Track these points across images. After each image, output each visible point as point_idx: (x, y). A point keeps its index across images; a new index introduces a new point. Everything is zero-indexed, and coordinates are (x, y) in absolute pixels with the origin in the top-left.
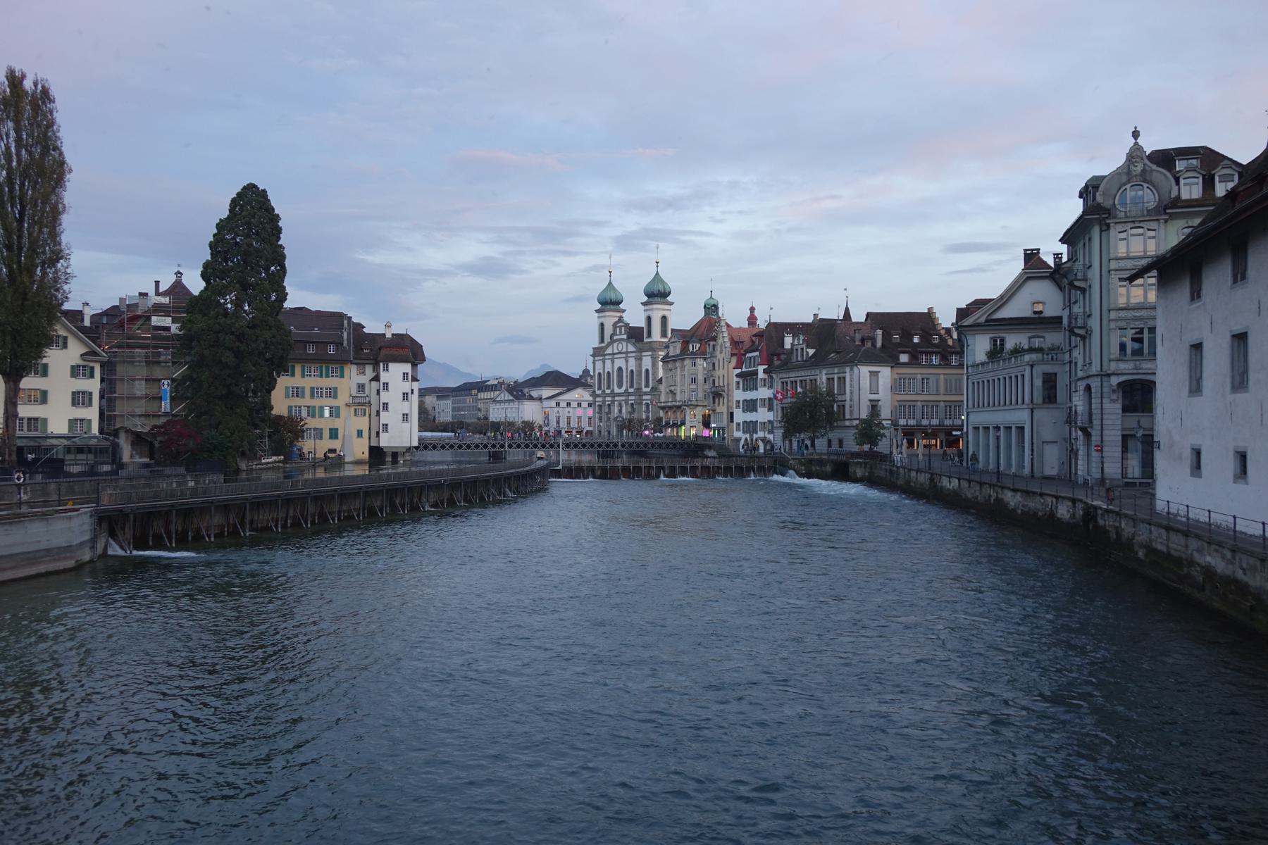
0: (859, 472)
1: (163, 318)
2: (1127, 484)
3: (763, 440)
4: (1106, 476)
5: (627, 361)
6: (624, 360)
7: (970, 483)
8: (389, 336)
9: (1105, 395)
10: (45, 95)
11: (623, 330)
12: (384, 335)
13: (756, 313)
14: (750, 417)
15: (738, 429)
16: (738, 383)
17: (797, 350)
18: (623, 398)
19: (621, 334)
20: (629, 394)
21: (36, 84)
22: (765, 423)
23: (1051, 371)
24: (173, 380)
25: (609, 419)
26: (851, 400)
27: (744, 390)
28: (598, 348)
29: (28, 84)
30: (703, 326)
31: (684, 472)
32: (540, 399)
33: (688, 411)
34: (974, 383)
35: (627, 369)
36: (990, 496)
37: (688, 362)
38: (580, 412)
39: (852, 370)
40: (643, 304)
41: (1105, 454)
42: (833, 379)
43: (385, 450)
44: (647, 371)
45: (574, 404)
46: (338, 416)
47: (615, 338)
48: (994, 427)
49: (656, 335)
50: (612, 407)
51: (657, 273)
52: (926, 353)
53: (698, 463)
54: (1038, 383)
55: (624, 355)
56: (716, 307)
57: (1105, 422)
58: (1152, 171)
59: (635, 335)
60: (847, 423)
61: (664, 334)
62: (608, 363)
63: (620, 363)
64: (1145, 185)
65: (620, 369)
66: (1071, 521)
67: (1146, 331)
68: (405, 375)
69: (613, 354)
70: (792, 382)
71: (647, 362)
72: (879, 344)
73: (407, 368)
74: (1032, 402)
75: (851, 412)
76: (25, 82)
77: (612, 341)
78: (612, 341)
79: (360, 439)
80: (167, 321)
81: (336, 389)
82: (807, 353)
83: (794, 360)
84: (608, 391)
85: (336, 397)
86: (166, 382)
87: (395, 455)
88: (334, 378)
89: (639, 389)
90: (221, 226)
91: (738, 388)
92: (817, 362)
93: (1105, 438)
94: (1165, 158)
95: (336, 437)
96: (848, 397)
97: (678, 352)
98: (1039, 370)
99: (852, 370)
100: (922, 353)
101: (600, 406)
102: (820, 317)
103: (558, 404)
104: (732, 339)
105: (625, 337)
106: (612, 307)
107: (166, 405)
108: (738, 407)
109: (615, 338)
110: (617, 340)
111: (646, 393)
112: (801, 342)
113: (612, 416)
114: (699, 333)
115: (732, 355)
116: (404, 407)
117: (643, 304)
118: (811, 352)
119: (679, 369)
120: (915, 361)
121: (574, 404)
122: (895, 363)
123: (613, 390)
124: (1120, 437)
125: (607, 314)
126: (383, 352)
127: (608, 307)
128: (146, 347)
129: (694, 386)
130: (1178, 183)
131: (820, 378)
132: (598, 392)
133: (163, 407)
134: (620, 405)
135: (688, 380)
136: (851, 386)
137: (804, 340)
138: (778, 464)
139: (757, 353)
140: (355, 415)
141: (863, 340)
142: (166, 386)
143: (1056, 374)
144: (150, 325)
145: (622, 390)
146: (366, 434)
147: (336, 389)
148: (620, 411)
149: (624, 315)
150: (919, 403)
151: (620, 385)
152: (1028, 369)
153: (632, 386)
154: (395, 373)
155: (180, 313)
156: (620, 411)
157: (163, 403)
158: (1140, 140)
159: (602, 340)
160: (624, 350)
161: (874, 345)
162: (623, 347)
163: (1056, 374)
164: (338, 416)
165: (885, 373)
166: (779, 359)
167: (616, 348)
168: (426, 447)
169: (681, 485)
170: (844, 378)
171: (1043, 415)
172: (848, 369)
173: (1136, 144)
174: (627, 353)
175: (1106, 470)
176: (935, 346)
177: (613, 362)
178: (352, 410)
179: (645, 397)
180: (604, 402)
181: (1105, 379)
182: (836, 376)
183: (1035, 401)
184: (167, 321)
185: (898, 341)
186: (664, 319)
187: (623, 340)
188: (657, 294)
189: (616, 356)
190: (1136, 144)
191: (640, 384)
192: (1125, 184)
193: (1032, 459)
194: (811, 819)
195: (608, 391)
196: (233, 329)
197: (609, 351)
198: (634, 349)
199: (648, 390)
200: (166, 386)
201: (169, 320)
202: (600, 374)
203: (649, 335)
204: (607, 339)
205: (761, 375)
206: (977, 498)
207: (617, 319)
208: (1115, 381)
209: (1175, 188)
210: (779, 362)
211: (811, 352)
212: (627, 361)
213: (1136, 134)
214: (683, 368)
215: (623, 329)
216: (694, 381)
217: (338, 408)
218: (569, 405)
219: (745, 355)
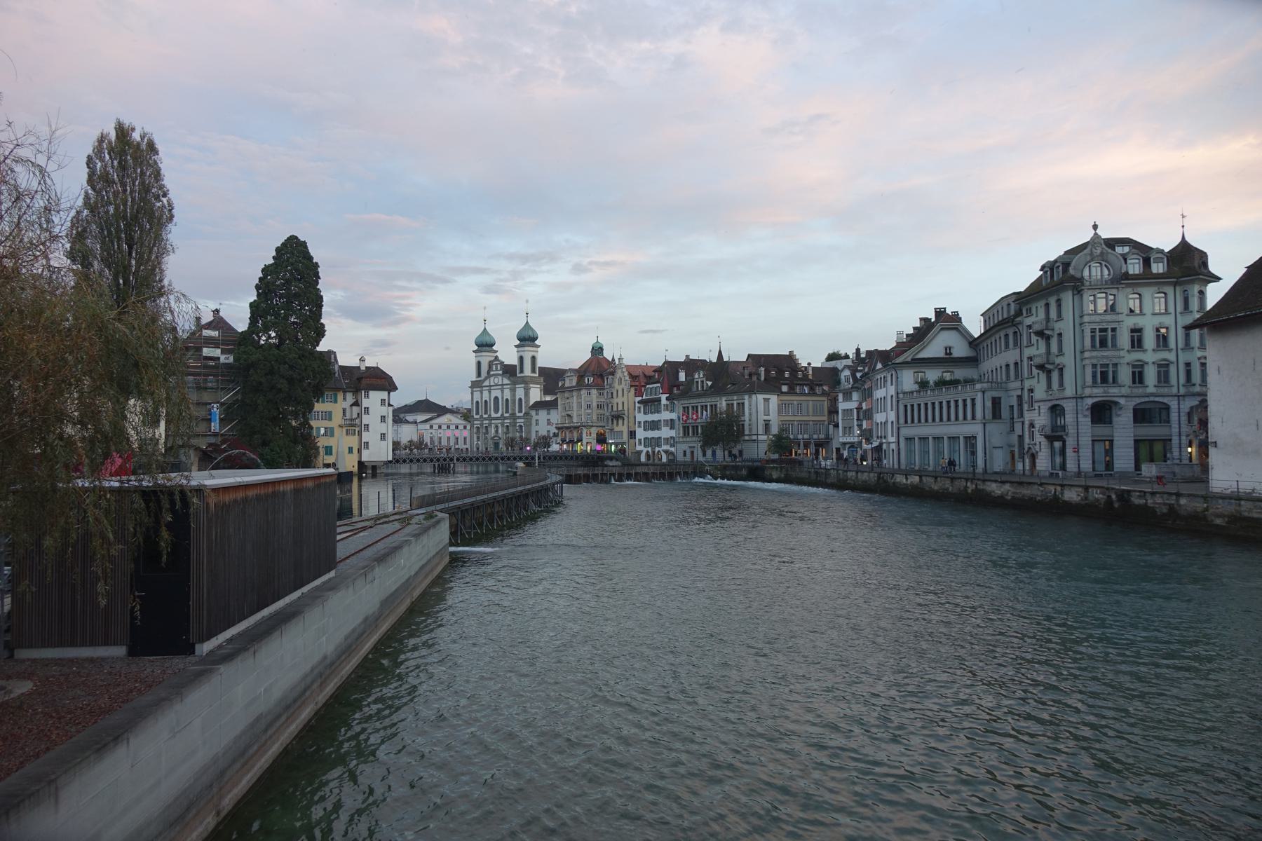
0: (775, 475)
1: (213, 349)
2: (1096, 476)
3: (666, 452)
4: (1082, 470)
5: (503, 392)
6: (500, 390)
7: (936, 478)
8: (363, 368)
9: (1079, 412)
10: (152, 147)
11: (499, 368)
12: (359, 367)
15: (640, 444)
16: (639, 408)
17: (697, 382)
19: (497, 370)
20: (506, 418)
21: (142, 138)
22: (667, 439)
23: (997, 396)
24: (222, 404)
25: (486, 438)
26: (750, 420)
27: (645, 413)
28: (476, 381)
29: (136, 136)
30: (593, 363)
31: (629, 477)
32: (415, 423)
33: (585, 431)
34: (906, 406)
35: (503, 398)
36: (966, 487)
37: (584, 392)
38: (457, 433)
39: (750, 397)
40: (516, 346)
41: (1080, 454)
42: (733, 404)
43: (366, 464)
44: (520, 400)
45: (444, 427)
46: (332, 435)
47: (492, 373)
48: (934, 438)
49: (527, 371)
51: (527, 322)
52: (800, 385)
53: (599, 471)
54: (989, 404)
56: (601, 349)
57: (1080, 431)
58: (1108, 253)
59: (509, 371)
60: (747, 438)
61: (533, 371)
62: (486, 394)
63: (496, 393)
64: (1104, 263)
65: (496, 398)
66: (1083, 503)
67: (1111, 366)
68: (383, 401)
69: (490, 386)
70: (693, 407)
71: (520, 393)
72: (763, 378)
73: (384, 395)
74: (984, 418)
75: (750, 430)
76: (134, 134)
77: (489, 376)
78: (489, 376)
79: (351, 455)
80: (217, 352)
81: (330, 413)
82: (707, 384)
83: (694, 389)
84: (485, 416)
85: (330, 419)
86: (215, 406)
87: (374, 468)
88: (329, 403)
89: (514, 414)
90: (266, 270)
91: (639, 412)
92: (717, 390)
93: (1080, 442)
94: (1112, 243)
95: (331, 454)
96: (747, 417)
97: (574, 383)
98: (989, 395)
99: (750, 397)
100: (797, 384)
101: (478, 428)
102: (691, 357)
103: (431, 427)
104: (630, 374)
105: (501, 372)
106: (487, 348)
107: (215, 426)
108: (640, 426)
109: (492, 373)
110: (493, 375)
111: (519, 418)
112: (701, 376)
113: (489, 436)
114: (591, 369)
115: (631, 386)
116: (382, 428)
117: (516, 346)
118: (710, 383)
119: (575, 398)
120: (792, 391)
121: (444, 427)
122: (776, 390)
123: (490, 415)
124: (1133, 442)
125: (484, 354)
126: (364, 382)
127: (484, 348)
128: (198, 374)
129: (589, 411)
130: (1126, 263)
131: (721, 404)
133: (213, 428)
134: (497, 427)
135: (584, 406)
136: (750, 409)
137: (704, 375)
138: (699, 471)
139: (659, 385)
140: (347, 434)
141: (750, 375)
142: (215, 409)
143: (1000, 398)
144: (201, 355)
145: (499, 415)
146: (355, 451)
147: (330, 413)
148: (497, 431)
149: (497, 354)
150: (796, 423)
151: (496, 411)
152: (980, 395)
153: (507, 412)
154: (373, 399)
155: (228, 345)
156: (497, 431)
157: (213, 424)
158: (1098, 231)
159: (479, 374)
160: (500, 383)
161: (759, 379)
162: (499, 380)
163: (1000, 398)
164: (332, 435)
165: (774, 399)
166: (678, 389)
167: (492, 381)
168: (397, 461)
169: (627, 486)
170: (743, 404)
171: (994, 428)
172: (746, 397)
173: (1096, 234)
174: (503, 385)
175: (1081, 466)
176: (801, 379)
177: (490, 393)
178: (344, 430)
179: (518, 421)
180: (482, 425)
181: (1079, 400)
182: (735, 403)
183: (987, 417)
184: (217, 352)
185: (774, 375)
186: (533, 358)
187: (499, 375)
188: (527, 338)
190: (1096, 234)
191: (514, 410)
192: (1090, 262)
193: (985, 460)
194: (927, 739)
195: (485, 416)
196: (287, 360)
197: (486, 383)
198: (509, 382)
199: (521, 414)
200: (215, 409)
201: (219, 351)
202: (477, 402)
203: (522, 371)
204: (484, 374)
205: (664, 401)
206: (948, 489)
207: (493, 358)
208: (1090, 401)
209: (1124, 266)
210: (679, 392)
211: (710, 383)
212: (503, 392)
213: (1095, 227)
214: (579, 396)
215: (499, 366)
216: (589, 406)
217: (332, 429)
218: (440, 427)
219: (645, 386)
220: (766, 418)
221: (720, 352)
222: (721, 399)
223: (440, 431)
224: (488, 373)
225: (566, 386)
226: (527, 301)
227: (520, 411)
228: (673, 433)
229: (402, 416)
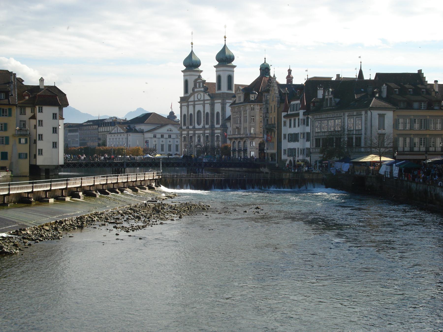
13: (293, 74)
14: (292, 145)
15: (285, 153)
18: (201, 132)
19: (200, 87)
39: (366, 113)
45: (166, 136)
47: (196, 90)
49: (224, 89)
50: (193, 138)
55: (202, 102)
62: (191, 108)
63: (199, 107)
73: (55, 110)
97: (242, 100)
99: (366, 113)
105: (202, 89)
111: (217, 129)
121: (166, 136)
132: (184, 128)
134: (199, 137)
145: (201, 126)
148: (199, 141)
151: (199, 124)
153: (207, 123)
156: (199, 141)
167: (196, 97)
174: (204, 100)
181: (116, 132)
186: (230, 79)
187: (201, 91)
189: (196, 103)
191: (212, 122)
195: (191, 127)
197: (192, 99)
202: (185, 115)
203: (219, 88)
205: (301, 116)
207: (197, 77)
218: (162, 136)
220: (381, 131)
221: (274, 75)
222: (344, 115)
223: (169, 140)
224: (193, 90)
225: (237, 102)
226: (225, 27)
227: (218, 123)
228: (308, 145)
229: (132, 126)
